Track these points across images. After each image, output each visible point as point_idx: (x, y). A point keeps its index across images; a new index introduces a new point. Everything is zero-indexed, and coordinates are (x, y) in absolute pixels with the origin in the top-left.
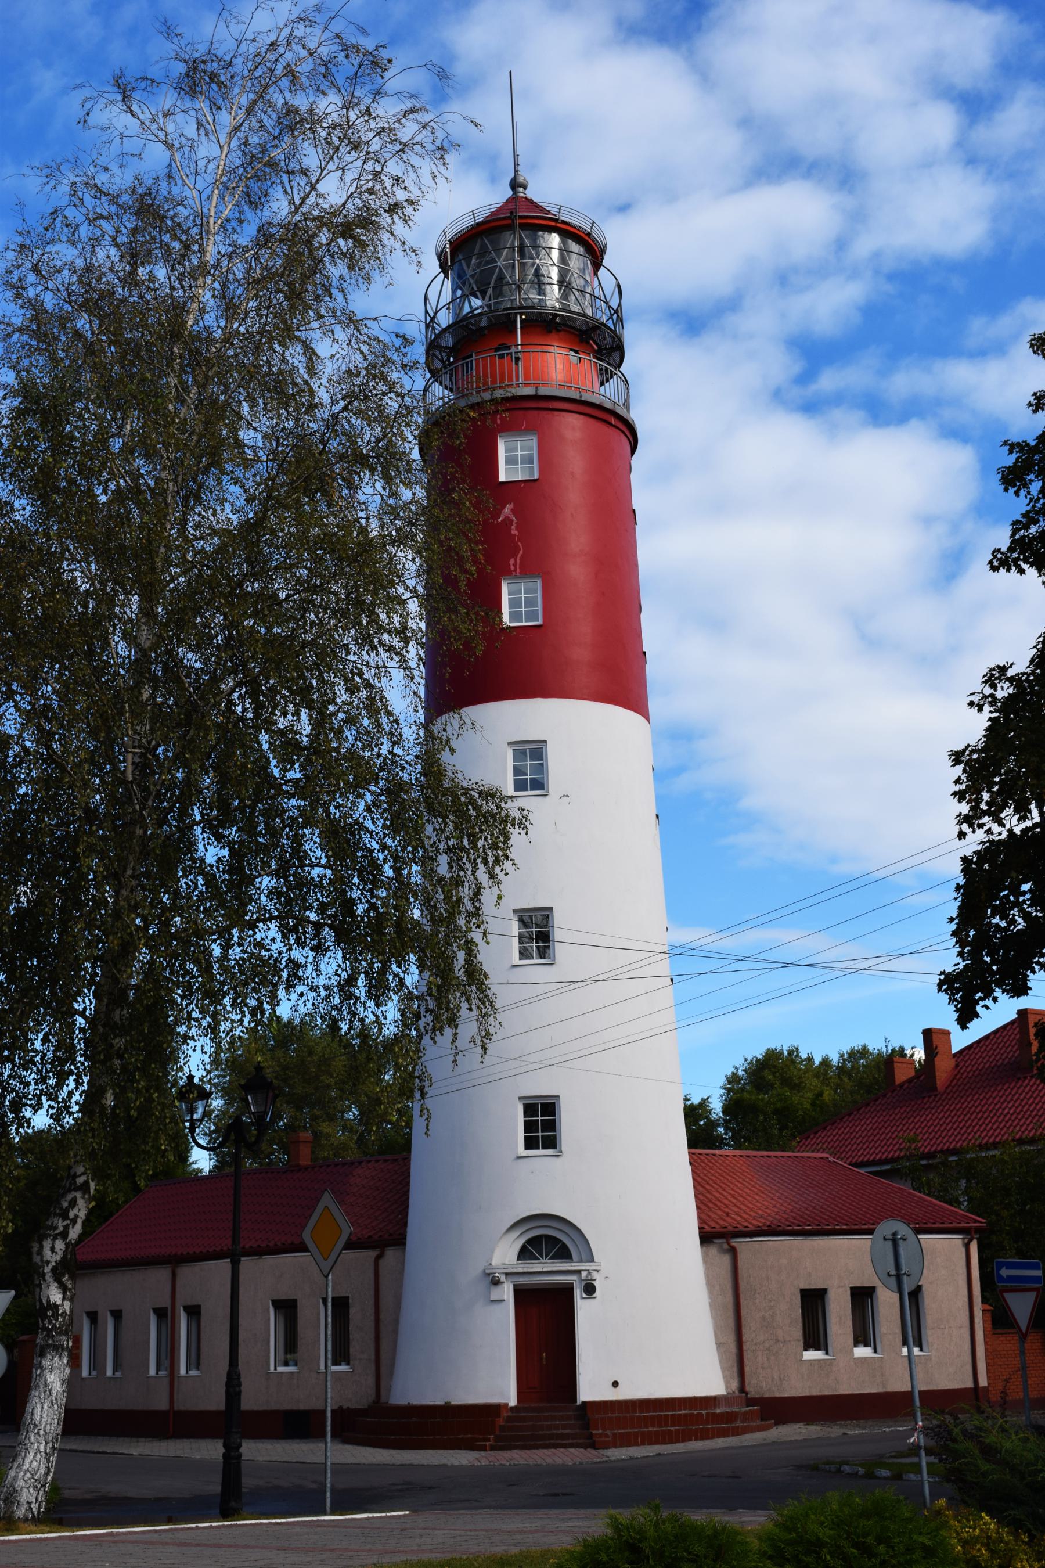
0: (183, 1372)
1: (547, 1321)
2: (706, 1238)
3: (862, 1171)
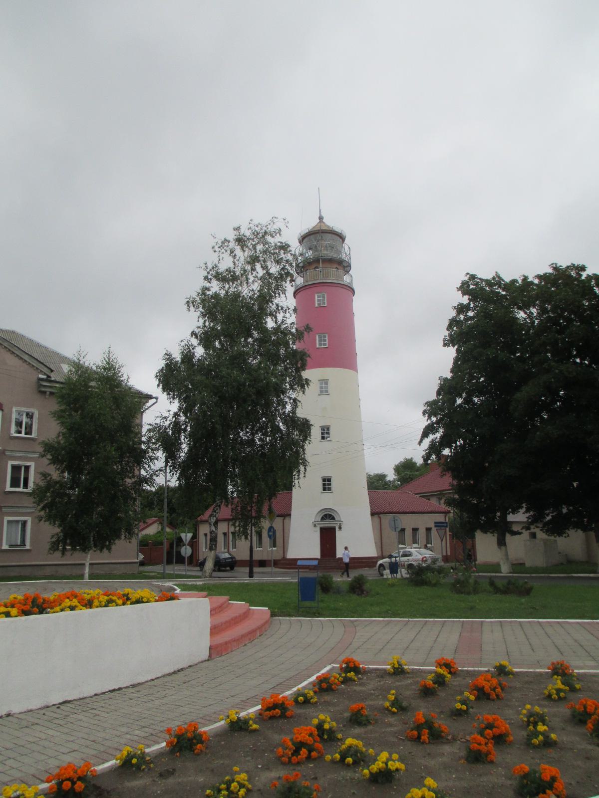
0: (231, 550)
1: (328, 537)
2: (373, 514)
3: (417, 496)
